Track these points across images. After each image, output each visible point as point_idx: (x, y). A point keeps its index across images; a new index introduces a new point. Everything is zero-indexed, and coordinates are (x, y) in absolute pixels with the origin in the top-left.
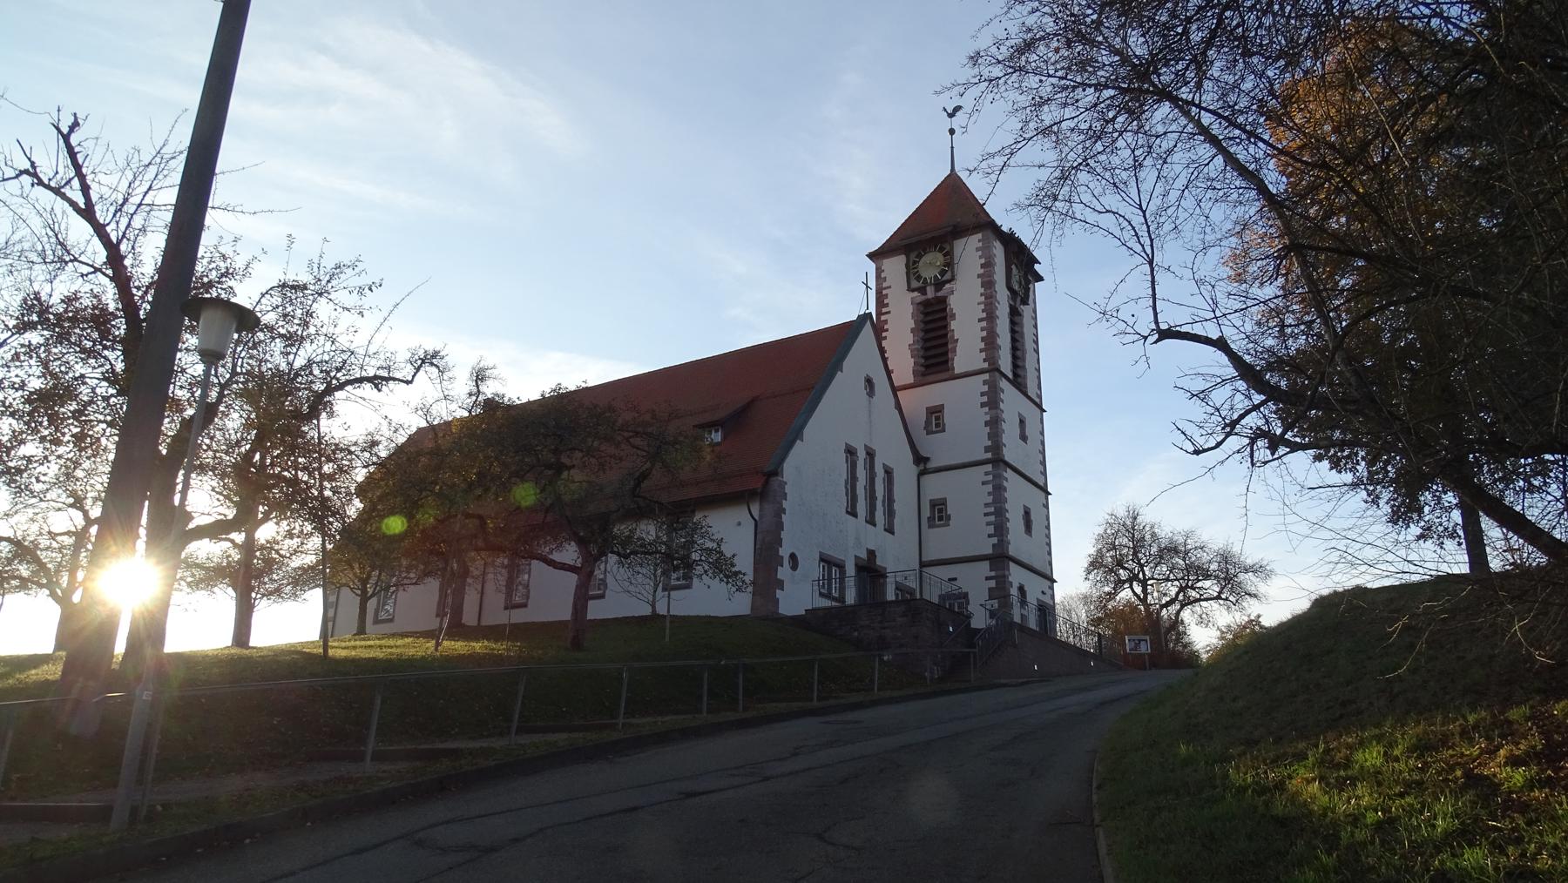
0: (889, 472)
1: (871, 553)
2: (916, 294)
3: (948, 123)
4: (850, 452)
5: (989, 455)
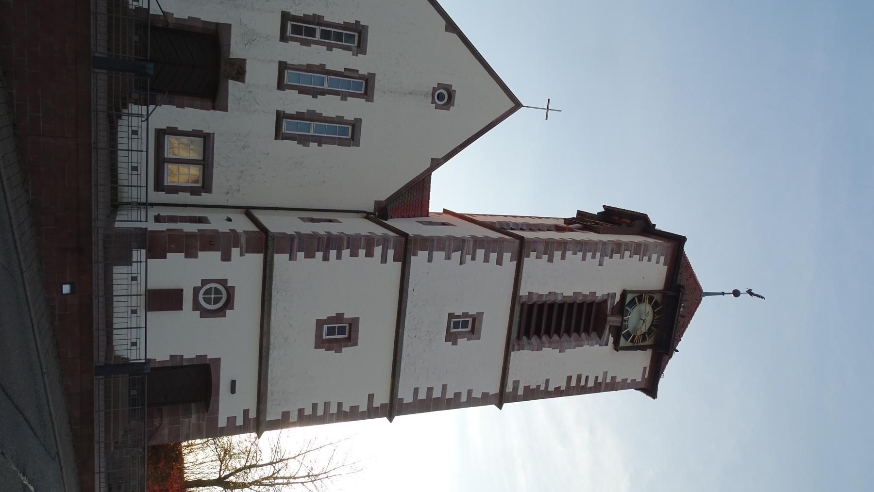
0: (349, 133)
1: (239, 71)
2: (617, 299)
3: (745, 297)
4: (354, 36)
5: (509, 388)
